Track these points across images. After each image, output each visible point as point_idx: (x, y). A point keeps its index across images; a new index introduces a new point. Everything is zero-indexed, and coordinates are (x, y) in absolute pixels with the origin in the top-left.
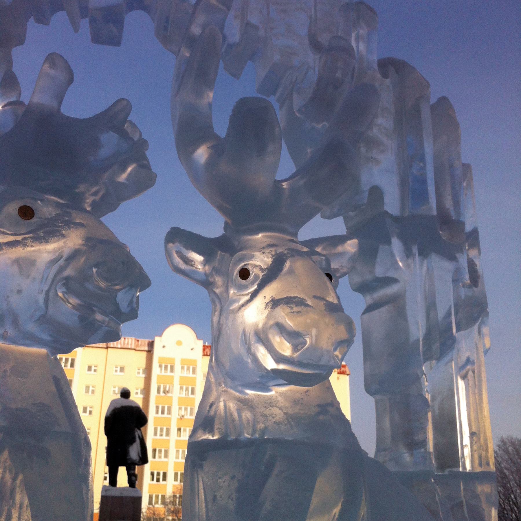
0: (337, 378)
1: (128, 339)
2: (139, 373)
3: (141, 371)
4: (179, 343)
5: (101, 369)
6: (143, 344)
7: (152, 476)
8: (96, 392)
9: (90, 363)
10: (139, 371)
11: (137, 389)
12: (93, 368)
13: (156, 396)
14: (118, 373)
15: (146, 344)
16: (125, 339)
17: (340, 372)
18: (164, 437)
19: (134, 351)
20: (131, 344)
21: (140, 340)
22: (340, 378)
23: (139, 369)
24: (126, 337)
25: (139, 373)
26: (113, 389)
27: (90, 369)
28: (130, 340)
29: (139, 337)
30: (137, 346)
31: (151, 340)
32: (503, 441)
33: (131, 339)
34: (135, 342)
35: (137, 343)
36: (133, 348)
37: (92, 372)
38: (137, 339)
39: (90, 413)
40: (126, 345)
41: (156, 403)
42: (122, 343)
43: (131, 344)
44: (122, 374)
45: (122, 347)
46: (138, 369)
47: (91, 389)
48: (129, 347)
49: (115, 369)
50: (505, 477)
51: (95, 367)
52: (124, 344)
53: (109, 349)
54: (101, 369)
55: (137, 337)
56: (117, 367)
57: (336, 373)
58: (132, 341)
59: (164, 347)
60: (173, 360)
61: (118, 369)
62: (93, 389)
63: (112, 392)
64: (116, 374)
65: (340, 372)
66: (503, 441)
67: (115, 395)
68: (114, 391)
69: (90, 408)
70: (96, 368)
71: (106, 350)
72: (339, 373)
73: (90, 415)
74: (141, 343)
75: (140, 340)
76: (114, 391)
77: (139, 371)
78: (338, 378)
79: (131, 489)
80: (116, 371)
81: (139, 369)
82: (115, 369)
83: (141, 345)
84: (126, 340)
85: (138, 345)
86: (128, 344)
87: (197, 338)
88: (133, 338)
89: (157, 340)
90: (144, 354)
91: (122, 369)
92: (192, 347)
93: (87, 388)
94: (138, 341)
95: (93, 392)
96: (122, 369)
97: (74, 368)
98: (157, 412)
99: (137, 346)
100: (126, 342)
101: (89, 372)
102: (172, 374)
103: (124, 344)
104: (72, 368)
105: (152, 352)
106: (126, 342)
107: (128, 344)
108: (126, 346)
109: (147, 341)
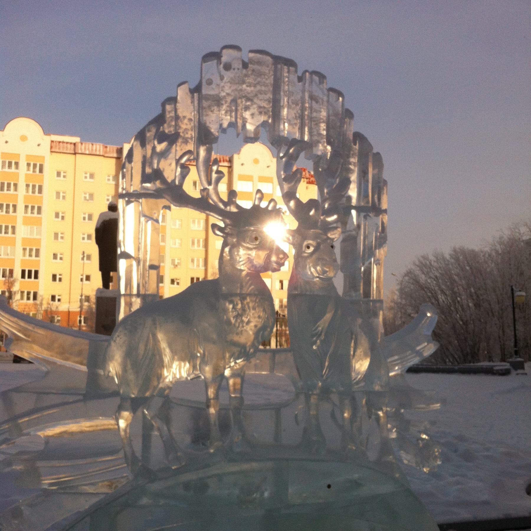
0: (306, 188)
1: (96, 145)
2: (109, 180)
3: (111, 178)
4: (256, 161)
5: (70, 175)
6: (112, 151)
7: (281, 284)
8: (67, 197)
9: (59, 169)
10: (109, 178)
11: (108, 196)
12: (62, 174)
13: (25, 196)
14: (88, 179)
15: (115, 151)
16: (93, 145)
17: (309, 182)
18: (10, 235)
19: (102, 158)
20: (100, 151)
21: (108, 146)
22: (309, 187)
23: (109, 176)
24: (94, 143)
25: (109, 180)
26: (84, 195)
27: (59, 174)
28: (98, 146)
29: (108, 144)
30: (106, 152)
31: (119, 147)
32: (455, 251)
33: (99, 145)
34: (103, 148)
35: (105, 149)
36: (101, 154)
37: (62, 178)
38: (105, 145)
39: (63, 218)
40: (94, 151)
41: (25, 202)
42: (90, 150)
43: (100, 151)
44: (92, 180)
45: (90, 153)
46: (85, 174)
47: (61, 194)
48: (98, 153)
49: (84, 175)
50: (453, 282)
51: (85, 174)
52: (92, 150)
53: (77, 155)
54: (70, 175)
55: (106, 143)
56: (110, 176)
57: (305, 182)
58: (100, 148)
59: (7, 142)
60: (18, 155)
61: (88, 175)
62: (64, 195)
63: (83, 199)
64: (86, 180)
65: (309, 182)
66: (455, 251)
67: (86, 201)
68: (85, 197)
69: (63, 213)
70: (65, 174)
71: (73, 156)
72: (308, 183)
73: (62, 221)
74: (110, 149)
75: (108, 146)
76: (85, 197)
77: (86, 175)
78: (307, 188)
79: (105, 290)
80: (86, 177)
81: (109, 176)
82: (107, 178)
83: (110, 151)
84: (94, 146)
85: (107, 151)
86: (96, 150)
87: (44, 133)
88: (101, 144)
89: (236, 157)
90: (114, 161)
91: (92, 176)
92: (268, 165)
93: (58, 194)
94: (106, 147)
95: (64, 197)
96: (92, 176)
97: (43, 174)
98: (26, 212)
99: (106, 152)
100: (94, 148)
101: (59, 178)
102: (17, 171)
103: (92, 150)
104: (41, 174)
105: (121, 159)
106: (94, 148)
107: (96, 150)
108: (94, 153)
109: (115, 147)
